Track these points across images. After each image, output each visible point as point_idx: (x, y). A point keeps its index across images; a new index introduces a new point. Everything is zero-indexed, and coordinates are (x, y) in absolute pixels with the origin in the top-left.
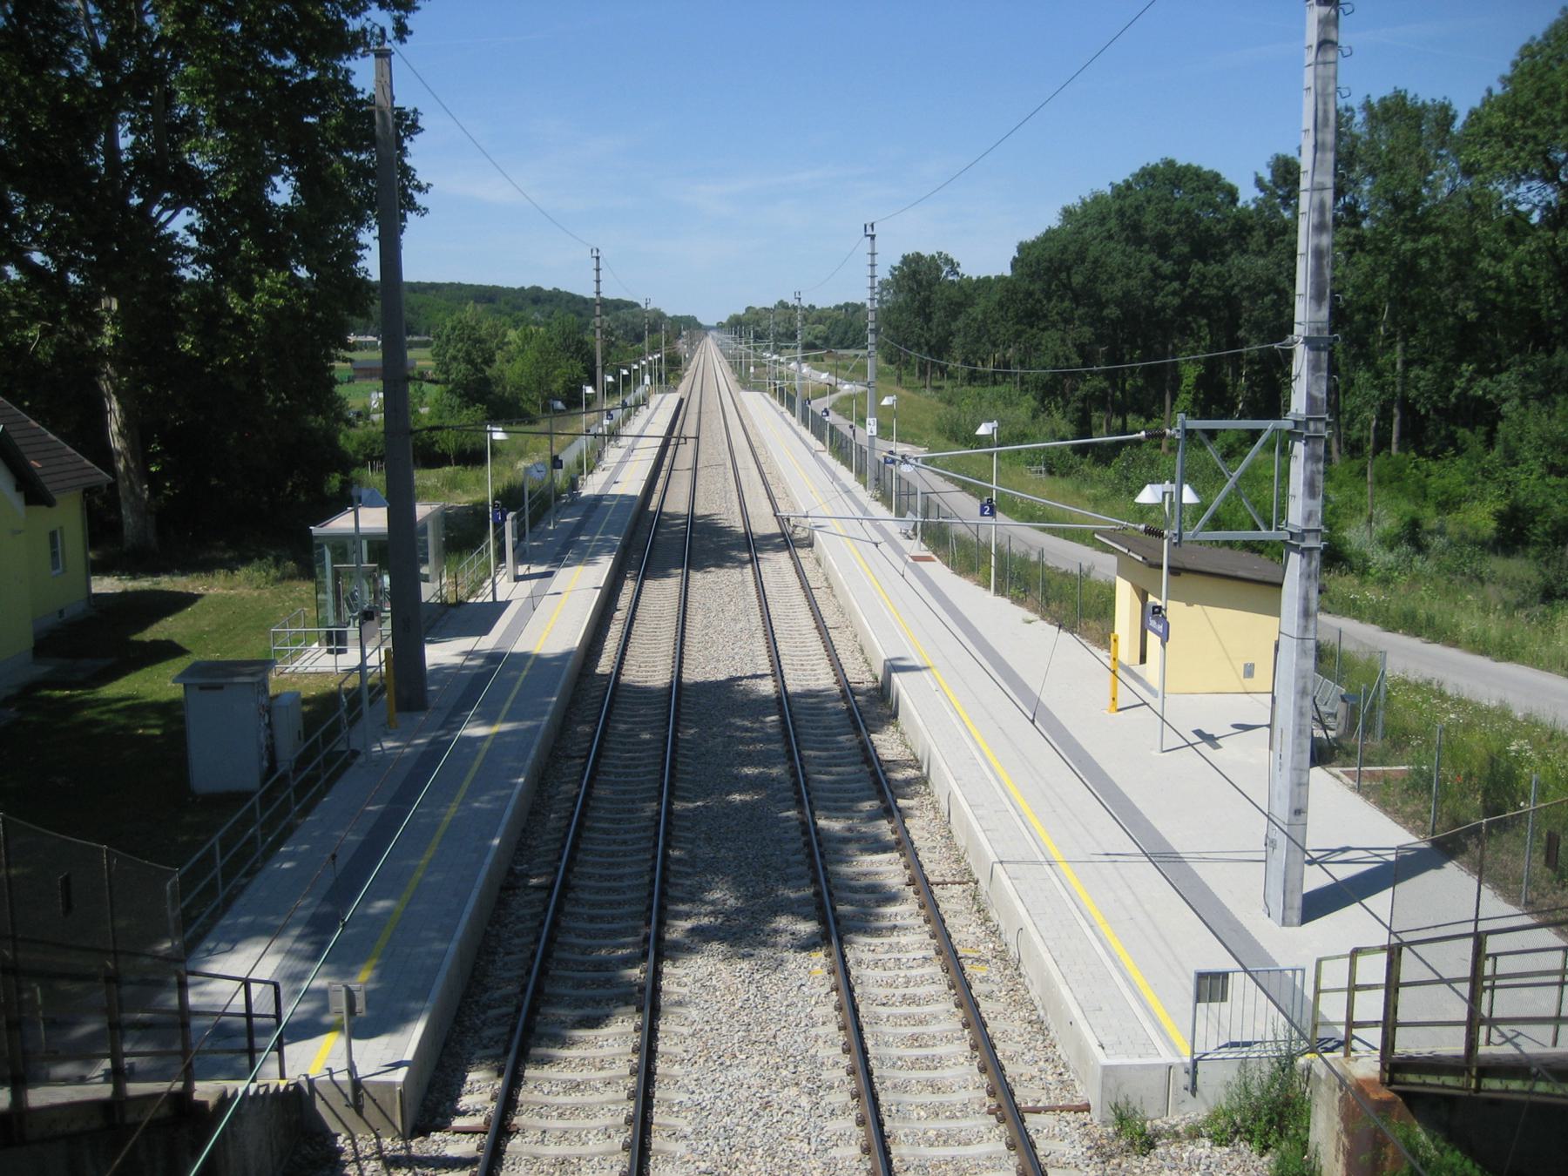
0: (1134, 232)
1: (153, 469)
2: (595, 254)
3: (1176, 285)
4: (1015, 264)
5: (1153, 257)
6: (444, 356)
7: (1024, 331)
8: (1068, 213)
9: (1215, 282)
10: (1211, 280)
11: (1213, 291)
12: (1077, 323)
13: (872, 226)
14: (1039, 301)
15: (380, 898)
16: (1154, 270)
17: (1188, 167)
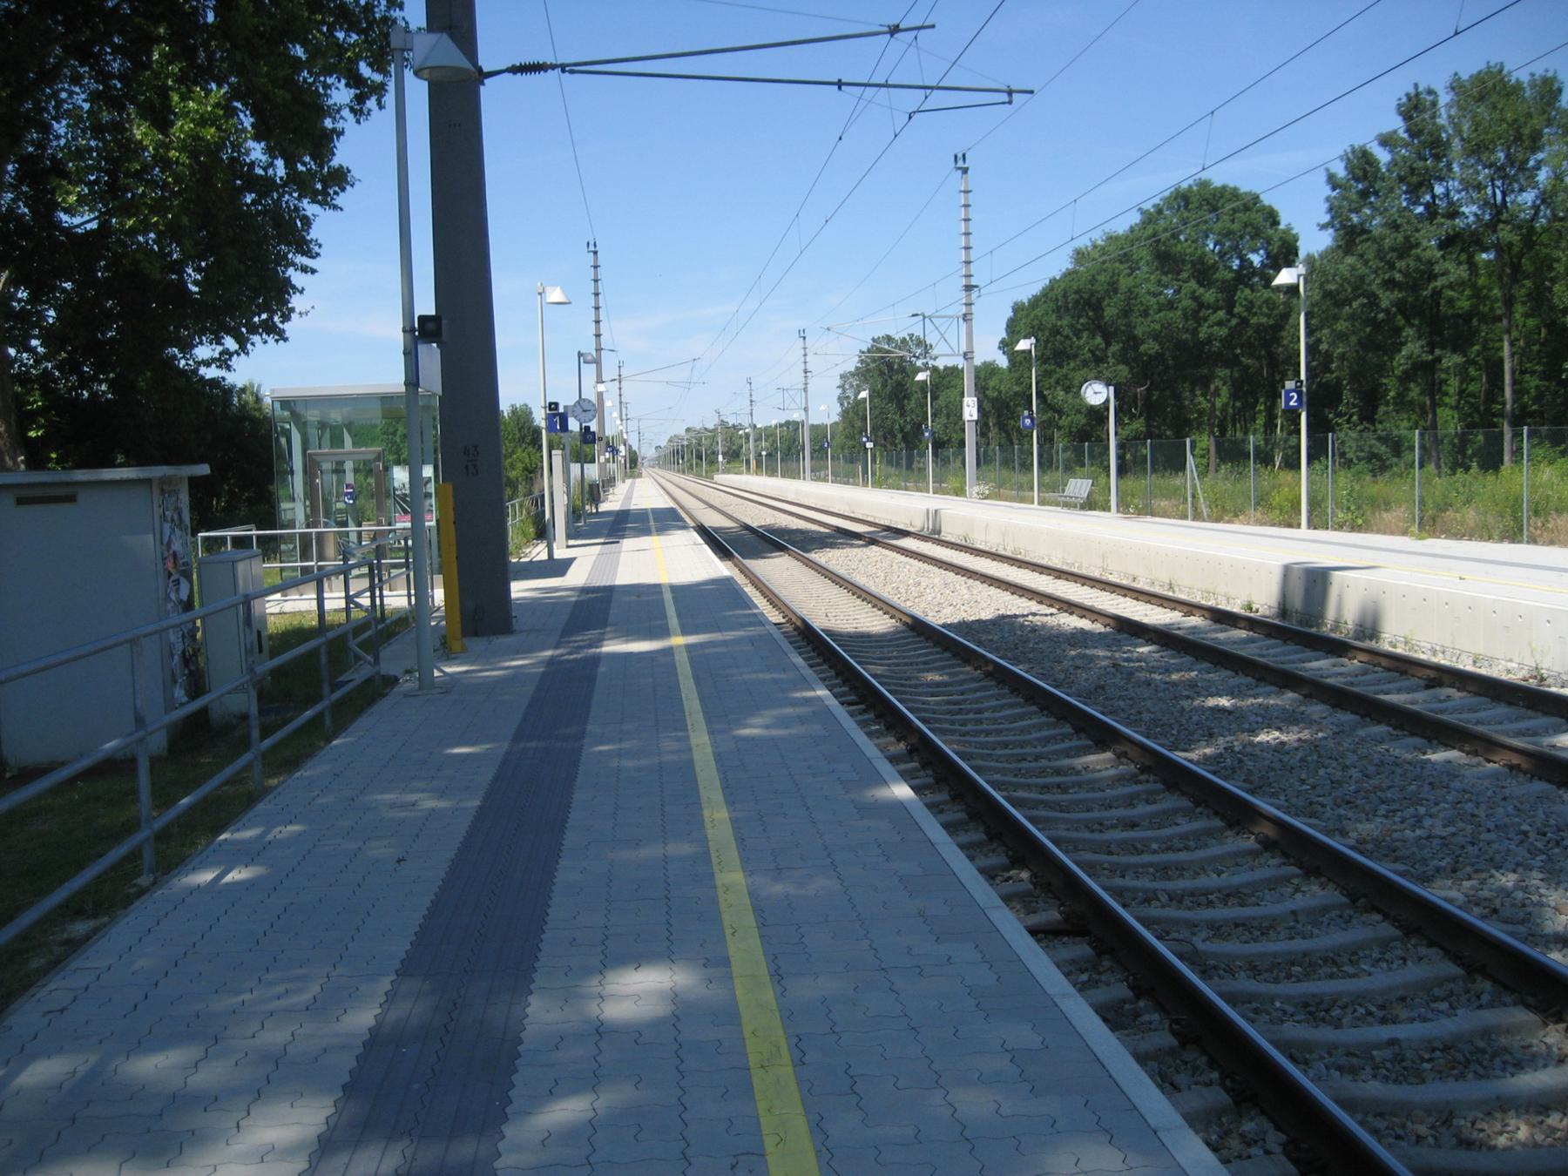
0: (1166, 260)
1: (32, 434)
2: (592, 248)
3: (1221, 314)
4: (1029, 300)
5: (1193, 284)
6: (394, 434)
7: (1054, 372)
8: (1080, 256)
9: (1265, 310)
10: (1260, 308)
11: (1264, 320)
12: (1111, 361)
13: (964, 156)
14: (1067, 337)
15: (638, 958)
16: (1195, 298)
17: (1224, 188)
